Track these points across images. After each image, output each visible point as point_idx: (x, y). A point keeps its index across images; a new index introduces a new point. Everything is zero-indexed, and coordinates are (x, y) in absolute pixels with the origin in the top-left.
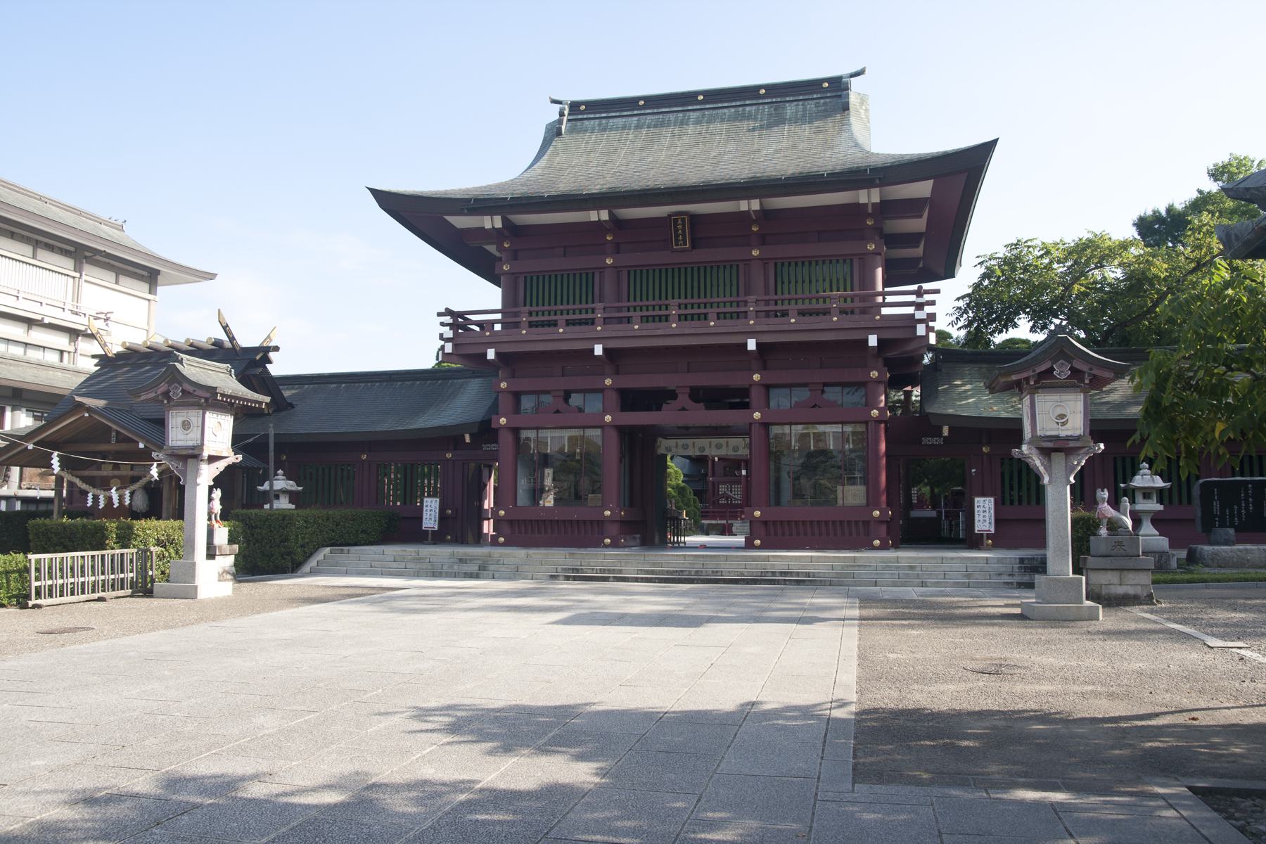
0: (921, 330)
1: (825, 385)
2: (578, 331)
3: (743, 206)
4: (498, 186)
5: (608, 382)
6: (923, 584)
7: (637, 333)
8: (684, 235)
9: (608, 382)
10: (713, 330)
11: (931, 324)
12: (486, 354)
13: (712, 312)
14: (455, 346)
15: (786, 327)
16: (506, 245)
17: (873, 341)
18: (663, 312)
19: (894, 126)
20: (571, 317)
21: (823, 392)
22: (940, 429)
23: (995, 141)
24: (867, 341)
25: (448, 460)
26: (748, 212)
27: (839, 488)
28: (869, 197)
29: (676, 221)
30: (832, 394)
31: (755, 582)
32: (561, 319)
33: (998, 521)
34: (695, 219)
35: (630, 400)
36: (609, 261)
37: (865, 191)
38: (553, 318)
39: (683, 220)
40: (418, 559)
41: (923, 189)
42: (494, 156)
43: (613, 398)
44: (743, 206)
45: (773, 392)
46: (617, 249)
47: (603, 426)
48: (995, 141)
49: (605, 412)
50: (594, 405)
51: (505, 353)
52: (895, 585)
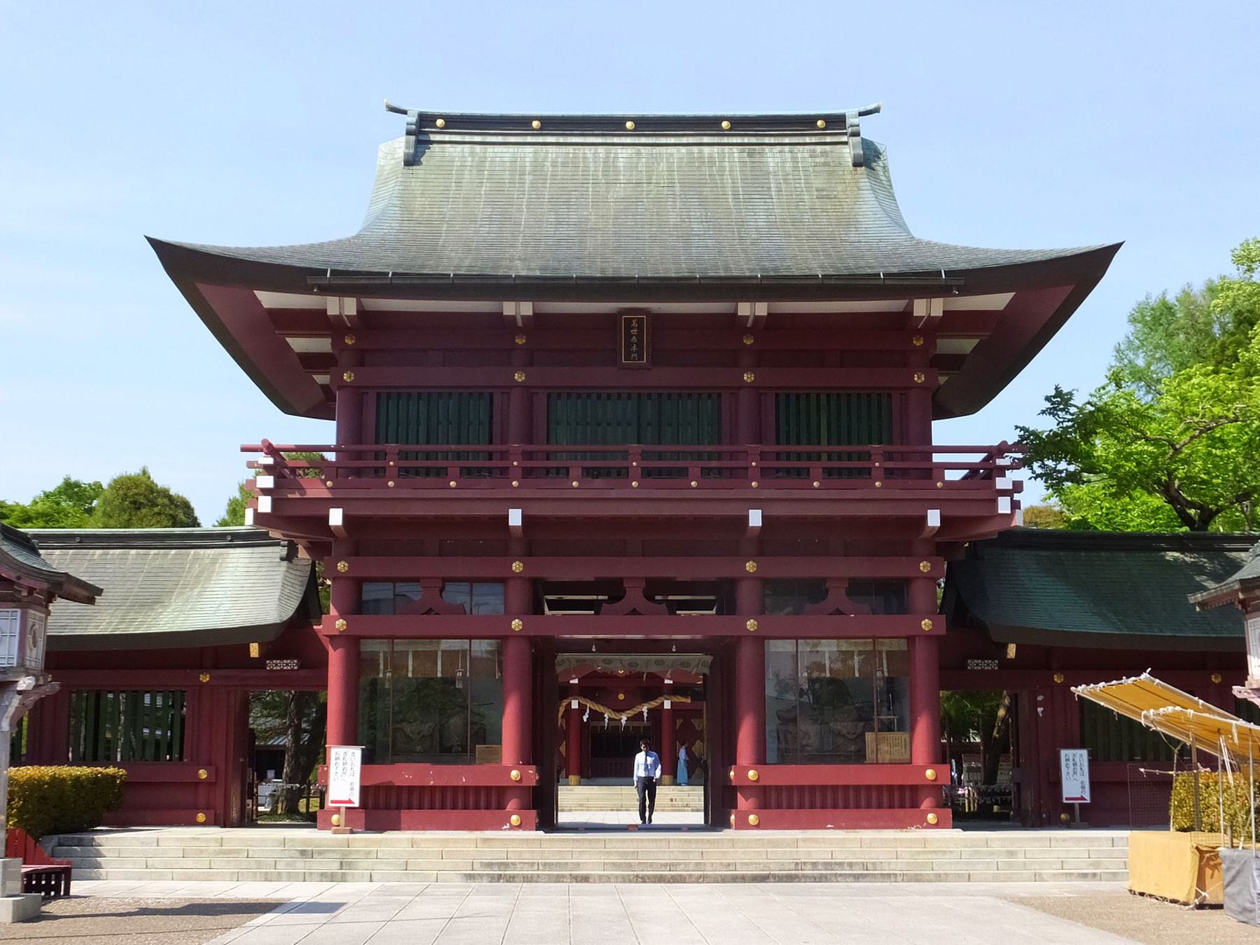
0: (1004, 506)
1: (445, 580)
2: (483, 488)
3: (509, 308)
4: (294, 250)
5: (517, 567)
6: (1037, 877)
7: (576, 496)
8: (640, 344)
9: (517, 567)
10: (693, 497)
11: (1017, 497)
12: (326, 518)
13: (816, 467)
14: (275, 503)
15: (380, 493)
16: (349, 341)
17: (934, 518)
18: (501, 464)
19: (955, 205)
20: (835, 464)
21: (442, 590)
22: (1004, 647)
23: (156, 244)
24: (747, 518)
25: (203, 685)
26: (513, 318)
27: (869, 736)
28: (927, 308)
29: (629, 321)
30: (456, 595)
31: (790, 878)
32: (695, 467)
33: (1094, 785)
34: (659, 320)
35: (538, 595)
36: (519, 377)
37: (513, 304)
38: (440, 463)
39: (640, 321)
40: (225, 852)
41: (998, 301)
42: (323, 200)
43: (518, 595)
44: (509, 308)
45: (450, 587)
46: (530, 362)
47: (504, 639)
48: (156, 244)
49: (510, 615)
50: (489, 602)
51: (535, 517)
52: (995, 879)
